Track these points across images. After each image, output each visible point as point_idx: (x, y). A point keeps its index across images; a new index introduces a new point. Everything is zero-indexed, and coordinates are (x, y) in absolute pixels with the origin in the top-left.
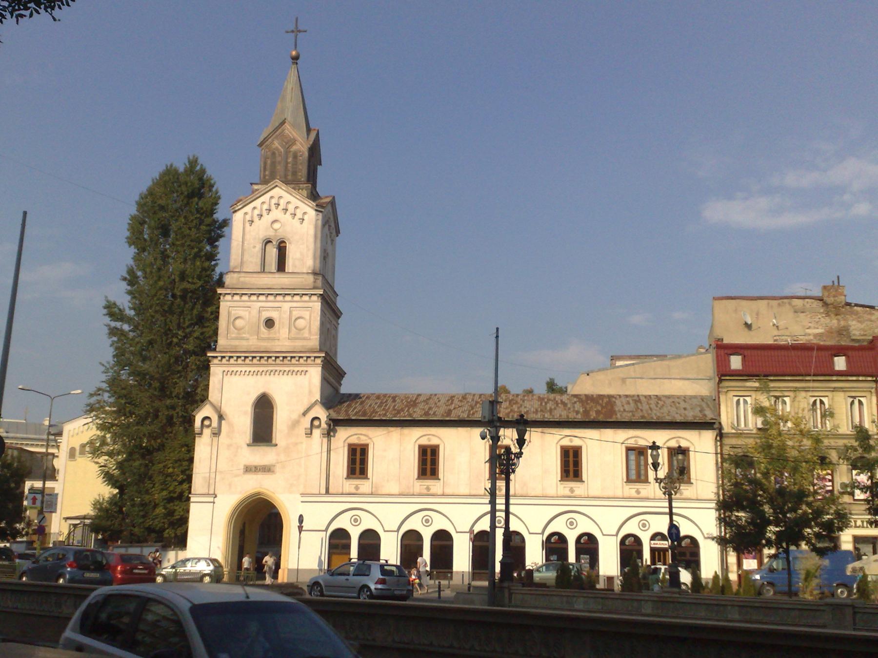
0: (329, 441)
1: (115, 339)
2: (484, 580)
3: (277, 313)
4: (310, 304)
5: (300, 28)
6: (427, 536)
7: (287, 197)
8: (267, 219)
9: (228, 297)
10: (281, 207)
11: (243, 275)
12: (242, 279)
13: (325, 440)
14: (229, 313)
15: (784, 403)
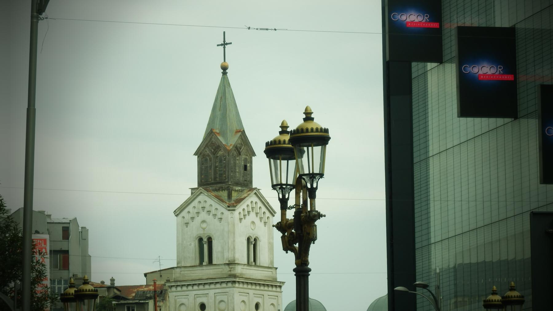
1: (438, 271)
2: (396, 290)
3: (206, 298)
4: (227, 290)
5: (227, 41)
7: (207, 199)
8: (198, 220)
9: (174, 289)
10: (206, 210)
11: (183, 269)
12: (183, 272)
14: (175, 301)
15: (304, 179)
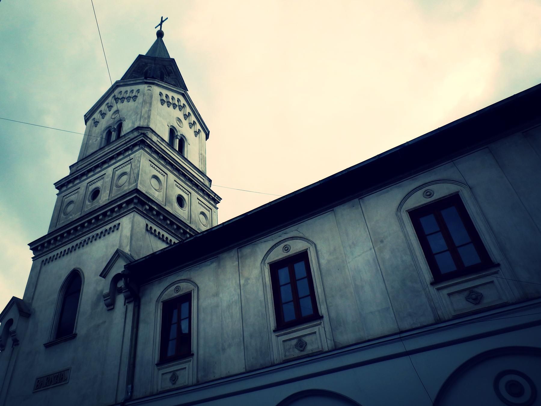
13: (131, 307)
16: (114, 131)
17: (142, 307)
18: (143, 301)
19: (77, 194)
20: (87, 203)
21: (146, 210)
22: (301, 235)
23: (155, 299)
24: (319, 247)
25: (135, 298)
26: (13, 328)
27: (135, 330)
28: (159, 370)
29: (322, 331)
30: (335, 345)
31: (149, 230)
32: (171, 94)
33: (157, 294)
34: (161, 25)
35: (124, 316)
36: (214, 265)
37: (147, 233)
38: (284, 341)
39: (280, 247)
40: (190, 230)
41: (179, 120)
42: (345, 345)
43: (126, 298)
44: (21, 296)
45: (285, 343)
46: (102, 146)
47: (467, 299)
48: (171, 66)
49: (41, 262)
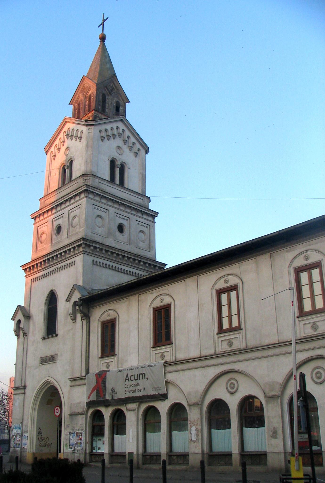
0: (89, 322)
6: (233, 403)
13: (85, 322)
16: (68, 168)
17: (91, 323)
18: (91, 319)
19: (47, 227)
20: (54, 236)
21: (91, 250)
22: (169, 293)
23: (98, 319)
24: (176, 303)
25: (87, 317)
26: (22, 325)
27: (88, 337)
28: (101, 361)
29: (172, 350)
30: (176, 359)
31: (95, 263)
32: (108, 127)
33: (99, 314)
34: (102, 24)
35: (81, 328)
36: (127, 303)
37: (95, 266)
38: (304, 324)
39: (223, 280)
40: (128, 254)
41: (119, 147)
42: (181, 360)
43: (82, 317)
44: (22, 304)
45: (305, 325)
46: (60, 186)
47: (228, 344)
48: (113, 82)
49: (30, 280)
